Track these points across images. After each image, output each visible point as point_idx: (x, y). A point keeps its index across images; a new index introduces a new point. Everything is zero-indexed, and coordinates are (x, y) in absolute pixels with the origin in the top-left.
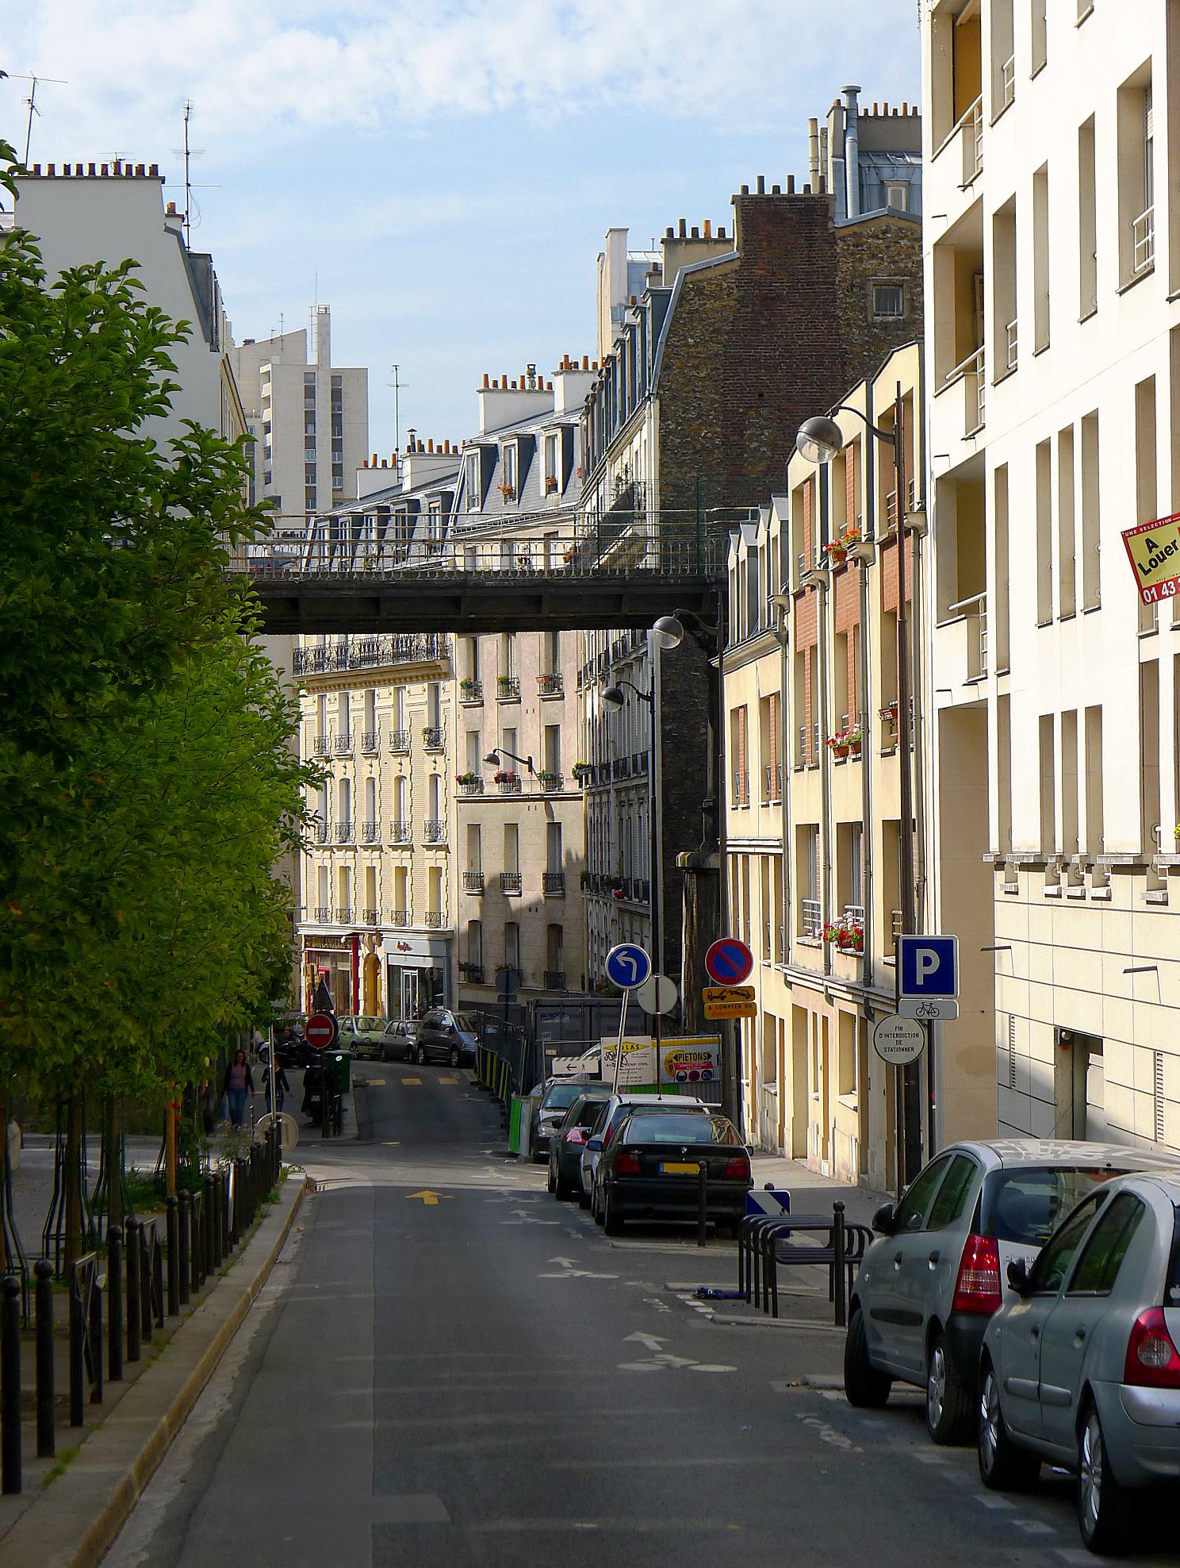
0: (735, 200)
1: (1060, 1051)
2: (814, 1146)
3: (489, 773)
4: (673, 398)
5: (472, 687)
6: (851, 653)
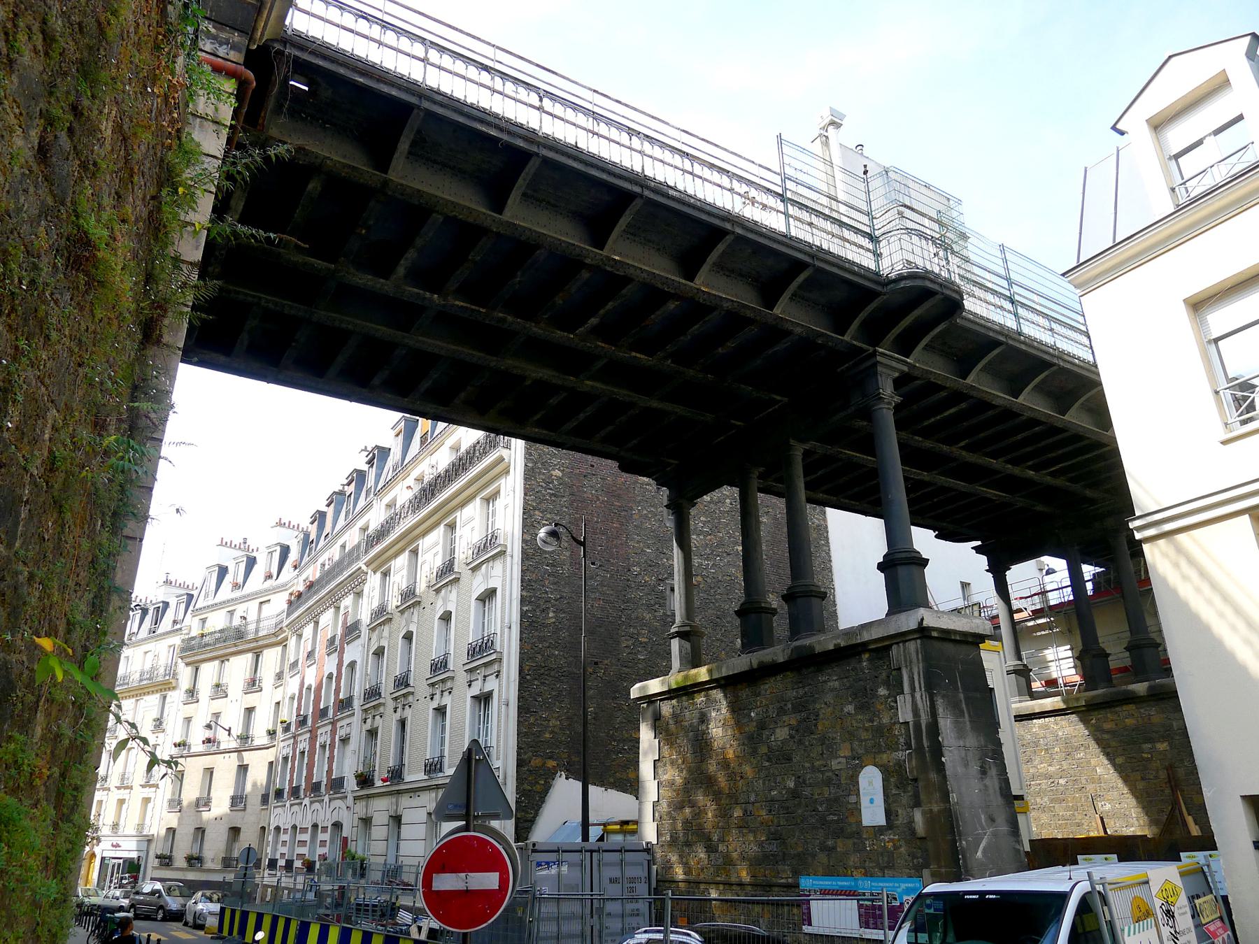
5: (192, 693)
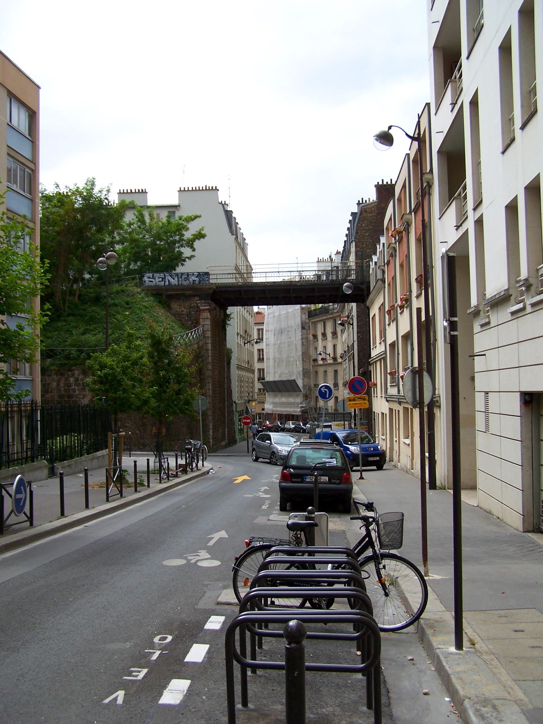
0: (375, 186)
1: (523, 406)
2: (395, 458)
3: (320, 357)
4: (359, 242)
6: (405, 271)
